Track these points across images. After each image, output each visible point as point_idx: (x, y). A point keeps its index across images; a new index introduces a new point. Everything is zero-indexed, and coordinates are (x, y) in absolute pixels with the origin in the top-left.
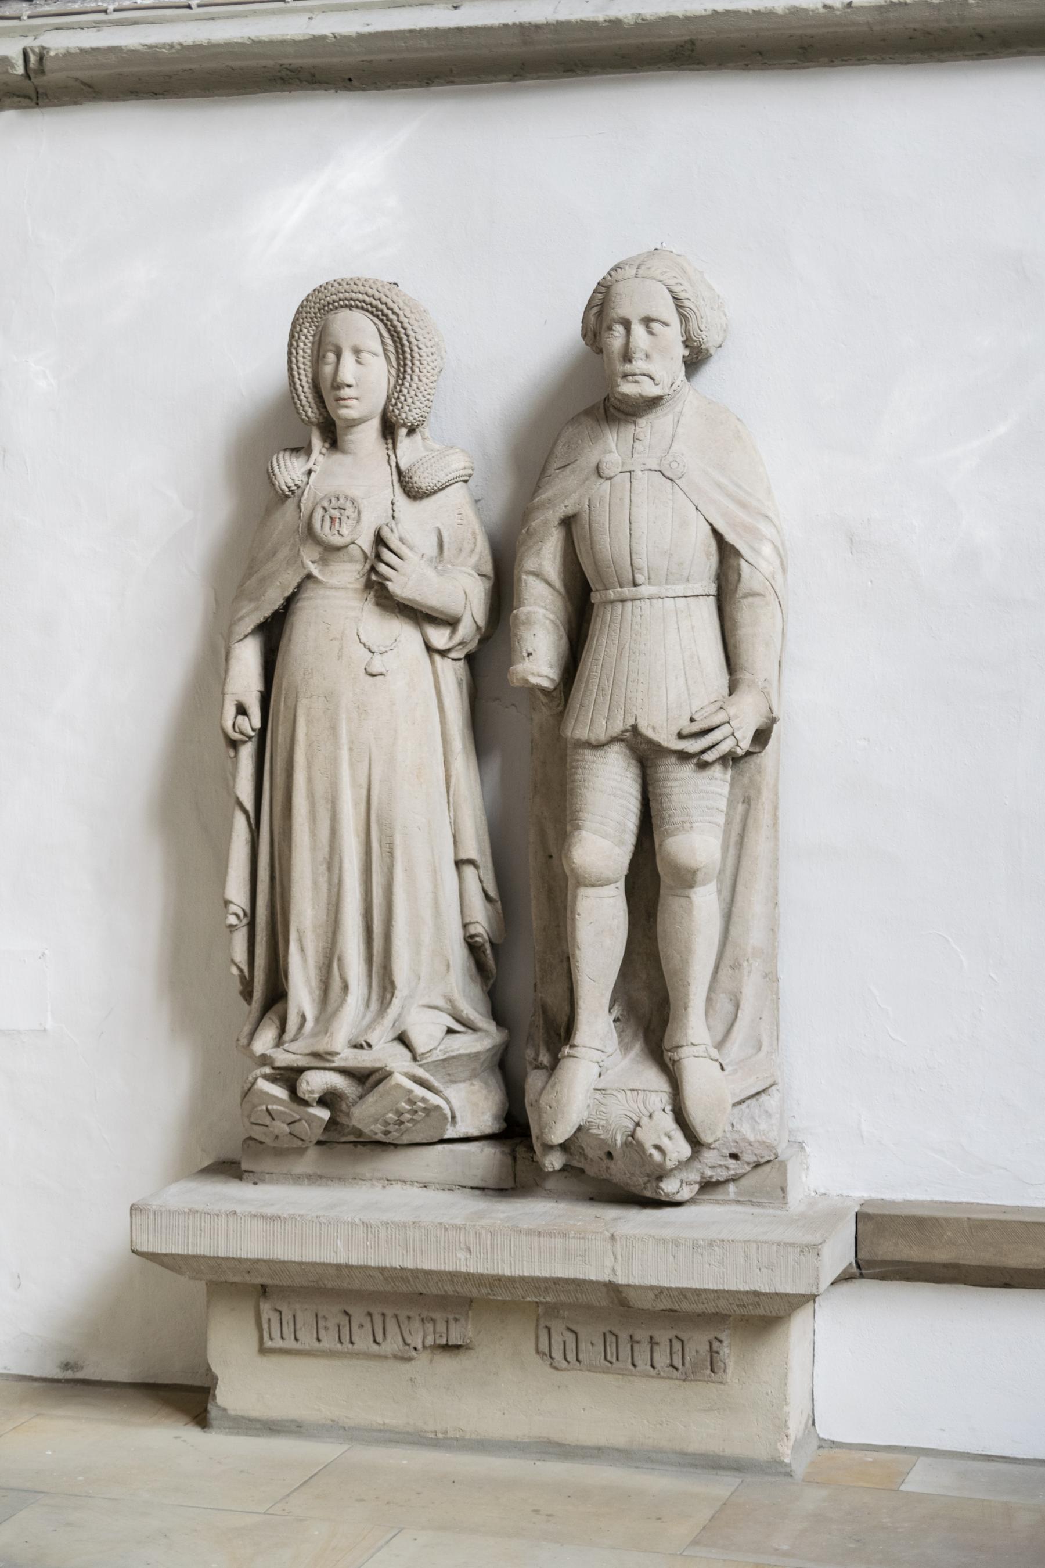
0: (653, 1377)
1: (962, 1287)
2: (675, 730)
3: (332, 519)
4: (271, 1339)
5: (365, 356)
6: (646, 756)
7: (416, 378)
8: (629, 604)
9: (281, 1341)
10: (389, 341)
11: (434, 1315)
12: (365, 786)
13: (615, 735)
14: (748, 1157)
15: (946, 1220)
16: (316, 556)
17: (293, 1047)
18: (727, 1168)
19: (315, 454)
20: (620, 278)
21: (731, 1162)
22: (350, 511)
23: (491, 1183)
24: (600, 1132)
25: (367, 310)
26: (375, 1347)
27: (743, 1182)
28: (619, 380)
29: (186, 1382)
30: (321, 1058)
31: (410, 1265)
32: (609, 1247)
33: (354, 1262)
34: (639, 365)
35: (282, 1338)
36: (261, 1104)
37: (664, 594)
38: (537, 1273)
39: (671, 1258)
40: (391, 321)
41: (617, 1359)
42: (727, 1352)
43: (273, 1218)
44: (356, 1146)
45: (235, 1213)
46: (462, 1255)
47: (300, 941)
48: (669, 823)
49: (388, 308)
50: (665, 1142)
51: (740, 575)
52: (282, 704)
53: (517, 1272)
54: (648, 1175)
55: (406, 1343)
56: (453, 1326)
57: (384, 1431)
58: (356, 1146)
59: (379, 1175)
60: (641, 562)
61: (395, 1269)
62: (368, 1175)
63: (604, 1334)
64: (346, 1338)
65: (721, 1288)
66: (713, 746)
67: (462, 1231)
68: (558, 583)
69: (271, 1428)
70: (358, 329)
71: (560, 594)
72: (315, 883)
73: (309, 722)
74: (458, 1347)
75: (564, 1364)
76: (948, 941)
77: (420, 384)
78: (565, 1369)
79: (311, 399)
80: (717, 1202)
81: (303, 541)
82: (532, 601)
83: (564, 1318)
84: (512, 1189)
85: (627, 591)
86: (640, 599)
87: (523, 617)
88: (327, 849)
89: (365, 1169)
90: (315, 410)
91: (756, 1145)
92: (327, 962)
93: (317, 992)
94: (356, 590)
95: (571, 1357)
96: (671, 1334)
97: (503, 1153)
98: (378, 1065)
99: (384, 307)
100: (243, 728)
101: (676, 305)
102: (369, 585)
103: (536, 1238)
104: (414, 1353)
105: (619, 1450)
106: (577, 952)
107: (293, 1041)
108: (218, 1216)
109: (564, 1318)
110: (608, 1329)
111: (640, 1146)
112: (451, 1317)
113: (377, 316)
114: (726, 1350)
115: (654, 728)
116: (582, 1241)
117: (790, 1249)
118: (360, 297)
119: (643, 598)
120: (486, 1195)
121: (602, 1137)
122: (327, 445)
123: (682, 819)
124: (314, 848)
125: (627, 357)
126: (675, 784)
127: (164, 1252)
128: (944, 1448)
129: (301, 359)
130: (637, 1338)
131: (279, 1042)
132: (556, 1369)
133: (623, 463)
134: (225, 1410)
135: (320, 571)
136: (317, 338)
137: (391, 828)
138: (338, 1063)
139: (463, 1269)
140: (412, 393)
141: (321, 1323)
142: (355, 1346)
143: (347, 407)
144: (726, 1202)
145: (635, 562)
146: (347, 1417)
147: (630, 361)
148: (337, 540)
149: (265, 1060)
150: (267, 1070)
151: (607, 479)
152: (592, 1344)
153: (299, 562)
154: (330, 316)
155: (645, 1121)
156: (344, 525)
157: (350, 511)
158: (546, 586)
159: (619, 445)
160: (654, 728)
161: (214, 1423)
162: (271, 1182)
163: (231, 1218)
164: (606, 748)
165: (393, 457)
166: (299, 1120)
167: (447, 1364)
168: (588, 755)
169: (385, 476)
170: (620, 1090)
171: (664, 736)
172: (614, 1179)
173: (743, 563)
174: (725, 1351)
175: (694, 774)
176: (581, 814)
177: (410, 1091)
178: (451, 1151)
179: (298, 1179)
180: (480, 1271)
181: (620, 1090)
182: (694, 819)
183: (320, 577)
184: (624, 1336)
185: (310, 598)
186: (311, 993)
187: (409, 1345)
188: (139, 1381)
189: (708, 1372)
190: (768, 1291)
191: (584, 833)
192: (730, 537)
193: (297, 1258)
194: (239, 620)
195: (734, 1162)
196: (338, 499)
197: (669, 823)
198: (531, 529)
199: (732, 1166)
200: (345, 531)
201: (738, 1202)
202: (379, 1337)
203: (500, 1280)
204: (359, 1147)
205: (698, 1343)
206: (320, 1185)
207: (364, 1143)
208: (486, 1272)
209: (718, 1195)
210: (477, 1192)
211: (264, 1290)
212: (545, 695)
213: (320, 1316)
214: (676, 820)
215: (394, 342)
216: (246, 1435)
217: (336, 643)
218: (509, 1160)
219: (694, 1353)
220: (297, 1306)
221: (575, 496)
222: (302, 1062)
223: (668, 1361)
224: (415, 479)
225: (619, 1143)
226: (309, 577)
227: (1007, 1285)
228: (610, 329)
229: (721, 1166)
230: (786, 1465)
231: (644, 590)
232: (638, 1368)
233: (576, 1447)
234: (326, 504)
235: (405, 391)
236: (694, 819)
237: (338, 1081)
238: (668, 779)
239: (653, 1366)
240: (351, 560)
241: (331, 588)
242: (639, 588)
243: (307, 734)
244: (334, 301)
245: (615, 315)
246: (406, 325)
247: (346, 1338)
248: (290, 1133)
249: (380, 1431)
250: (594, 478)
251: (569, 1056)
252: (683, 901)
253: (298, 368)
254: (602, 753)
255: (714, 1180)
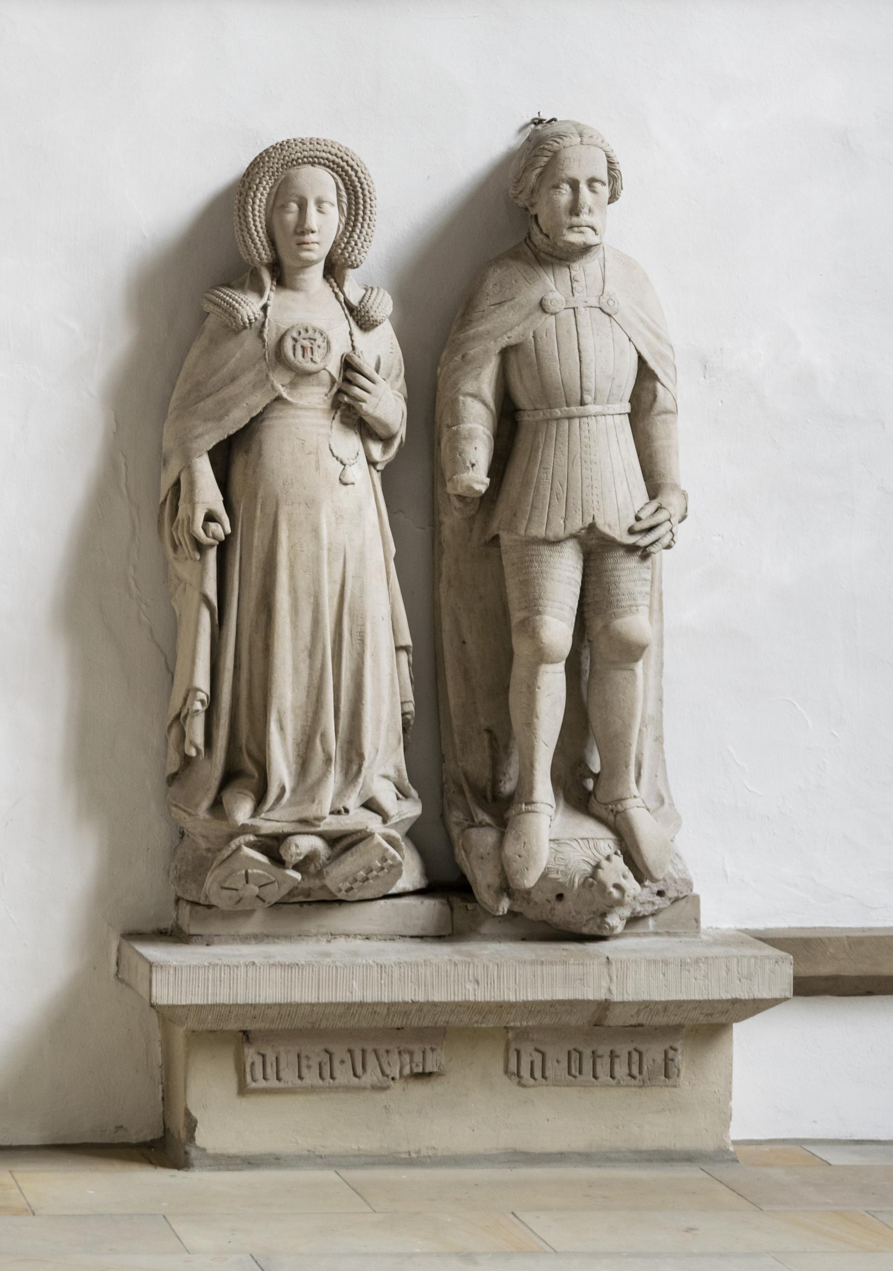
0: (612, 1086)
1: (828, 997)
2: (625, 527)
3: (303, 348)
4: (254, 1080)
5: (326, 206)
6: (596, 549)
7: (366, 226)
8: (577, 421)
9: (264, 1082)
10: (344, 193)
11: (411, 1047)
12: (339, 582)
13: (574, 532)
14: (671, 894)
15: (829, 939)
16: (287, 380)
17: (273, 815)
18: (653, 904)
19: (267, 292)
20: (567, 144)
21: (657, 899)
22: (320, 341)
23: (431, 931)
24: (559, 876)
25: (329, 167)
26: (356, 1080)
27: (661, 916)
28: (565, 231)
29: (94, 1141)
30: (307, 824)
31: (421, 998)
32: (606, 970)
33: (369, 999)
34: (585, 218)
35: (265, 1078)
36: (240, 870)
37: (607, 411)
38: (540, 997)
39: (662, 976)
40: (350, 176)
41: (580, 1073)
42: (681, 1059)
43: (290, 966)
44: (302, 906)
45: (254, 963)
46: (470, 986)
47: (280, 722)
48: (618, 607)
49: (348, 165)
50: (623, 882)
51: (655, 397)
52: (259, 511)
53: (522, 997)
54: (594, 913)
55: (383, 1073)
56: (430, 1056)
57: (360, 1156)
58: (302, 906)
59: (324, 930)
60: (590, 384)
61: (407, 1003)
62: (313, 931)
63: (569, 1053)
64: (327, 1074)
65: (706, 998)
66: (657, 541)
67: (471, 966)
68: (492, 404)
69: (250, 1162)
70: (320, 183)
71: (491, 411)
72: (296, 669)
73: (291, 527)
74: (430, 1074)
75: (532, 1081)
76: (795, 705)
77: (369, 231)
78: (533, 1086)
79: (265, 243)
80: (638, 935)
81: (272, 367)
82: (471, 419)
83: (533, 1040)
84: (450, 935)
85: (575, 410)
86: (587, 417)
87: (464, 433)
88: (308, 638)
89: (311, 926)
90: (269, 253)
91: (679, 882)
92: (305, 739)
93: (294, 766)
94: (324, 409)
95: (538, 1074)
96: (630, 1047)
97: (443, 904)
98: (359, 827)
99: (344, 164)
100: (216, 533)
101: (609, 168)
102: (336, 405)
103: (539, 967)
104: (392, 1082)
105: (579, 1154)
106: (535, 720)
107: (268, 811)
108: (237, 967)
109: (533, 1040)
110: (574, 1046)
111: (602, 886)
112: (428, 1047)
113: (337, 172)
114: (680, 1057)
115: (610, 526)
116: (581, 967)
117: (767, 961)
118: (324, 155)
119: (590, 416)
120: (426, 941)
121: (561, 880)
122: (275, 283)
123: (629, 603)
124: (295, 638)
125: (575, 209)
126: (623, 573)
127: (184, 1003)
128: (817, 1137)
129: (257, 208)
130: (600, 1052)
131: (256, 812)
132: (524, 1086)
133: (567, 301)
134: (204, 1150)
135: (288, 394)
136: (275, 190)
137: (363, 618)
138: (323, 827)
139: (472, 999)
140: (363, 238)
141: (304, 1062)
142: (337, 1081)
143: (309, 250)
144: (646, 934)
145: (584, 385)
146: (323, 1147)
147: (578, 215)
148: (310, 366)
149: (244, 829)
150: (252, 838)
151: (552, 314)
152: (558, 1062)
153: (269, 386)
154: (292, 171)
155: (604, 863)
156: (315, 353)
157: (320, 341)
158: (483, 406)
159: (558, 285)
160: (610, 526)
161: (195, 1162)
162: (221, 943)
163: (250, 969)
164: (562, 544)
165: (340, 294)
166: (273, 882)
167: (419, 1091)
168: (545, 551)
169: (338, 312)
170: (571, 840)
171: (618, 532)
172: (564, 920)
173: (659, 386)
174: (679, 1058)
175: (639, 565)
176: (541, 601)
177: (387, 850)
178: (393, 905)
179: (246, 939)
180: (488, 999)
181: (571, 840)
182: (639, 602)
183: (289, 399)
184: (587, 1053)
185: (276, 418)
186: (288, 767)
187: (387, 1076)
188: (50, 1143)
189: (663, 1078)
190: (747, 998)
191: (546, 618)
192: (652, 364)
193: (313, 999)
194: (197, 437)
195: (659, 898)
196: (307, 331)
197: (618, 607)
198: (469, 357)
199: (657, 902)
200: (317, 358)
201: (656, 934)
202: (359, 1070)
203: (501, 1007)
204: (305, 906)
205: (654, 1053)
206: (268, 943)
207: (310, 903)
208: (493, 999)
209: (639, 928)
210: (418, 940)
211: (246, 1036)
212: (460, 501)
213: (303, 1056)
214: (624, 604)
215: (348, 194)
216: (228, 1170)
217: (313, 456)
218: (447, 909)
219: (651, 1062)
220: (282, 1049)
221: (519, 329)
222: (287, 828)
223: (627, 1071)
224: (372, 313)
225: (576, 885)
226: (279, 399)
227: (869, 993)
228: (557, 187)
229: (649, 902)
230: (731, 1153)
231: (591, 408)
232: (600, 1080)
233: (539, 1154)
234: (295, 335)
235: (356, 237)
236: (639, 602)
237: (317, 843)
238: (616, 569)
239: (612, 1077)
240: (320, 384)
241: (302, 409)
242: (587, 407)
243: (289, 537)
244: (298, 158)
245: (563, 176)
246: (363, 180)
247: (327, 1074)
248: (257, 896)
249: (355, 1156)
250: (539, 313)
251: (528, 812)
252: (626, 674)
253: (254, 215)
254: (559, 548)
255: (641, 915)
